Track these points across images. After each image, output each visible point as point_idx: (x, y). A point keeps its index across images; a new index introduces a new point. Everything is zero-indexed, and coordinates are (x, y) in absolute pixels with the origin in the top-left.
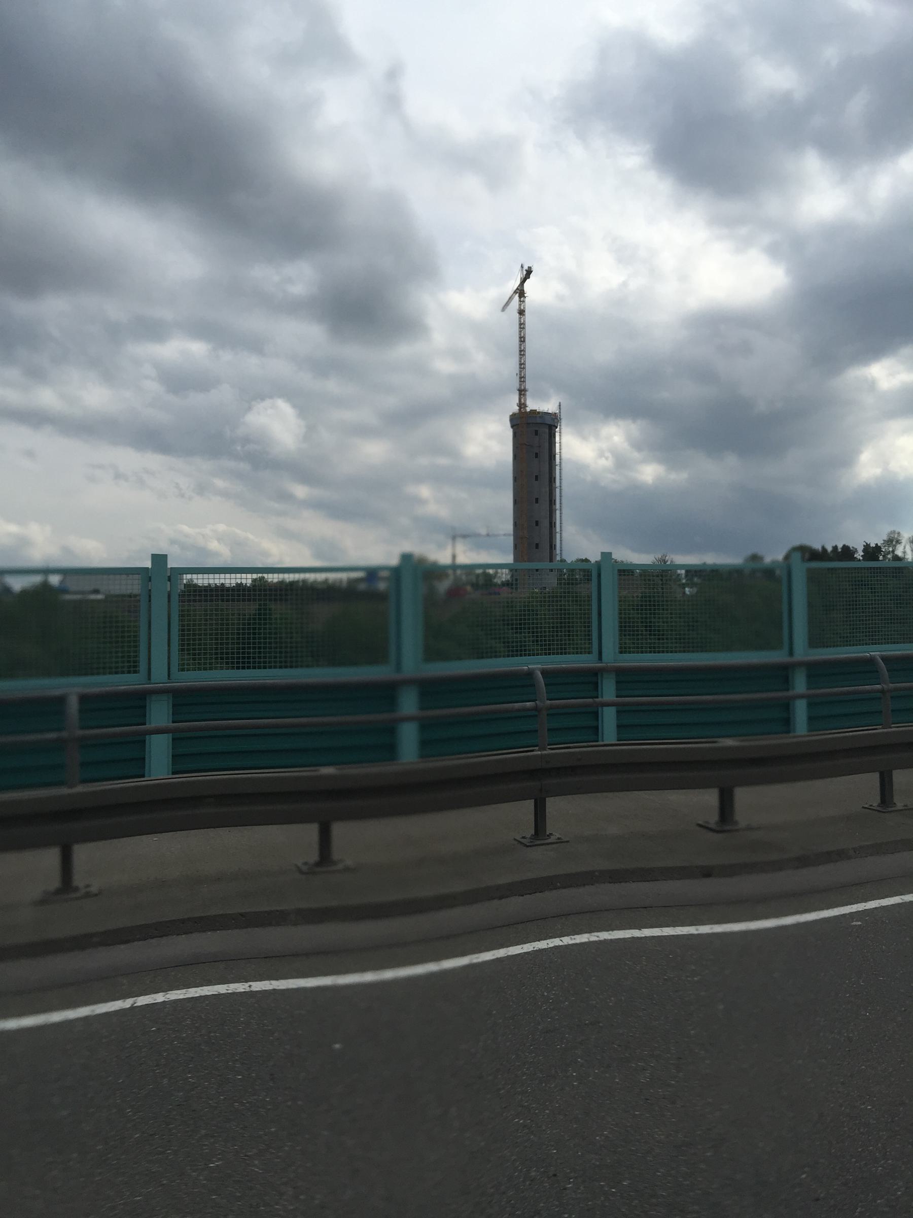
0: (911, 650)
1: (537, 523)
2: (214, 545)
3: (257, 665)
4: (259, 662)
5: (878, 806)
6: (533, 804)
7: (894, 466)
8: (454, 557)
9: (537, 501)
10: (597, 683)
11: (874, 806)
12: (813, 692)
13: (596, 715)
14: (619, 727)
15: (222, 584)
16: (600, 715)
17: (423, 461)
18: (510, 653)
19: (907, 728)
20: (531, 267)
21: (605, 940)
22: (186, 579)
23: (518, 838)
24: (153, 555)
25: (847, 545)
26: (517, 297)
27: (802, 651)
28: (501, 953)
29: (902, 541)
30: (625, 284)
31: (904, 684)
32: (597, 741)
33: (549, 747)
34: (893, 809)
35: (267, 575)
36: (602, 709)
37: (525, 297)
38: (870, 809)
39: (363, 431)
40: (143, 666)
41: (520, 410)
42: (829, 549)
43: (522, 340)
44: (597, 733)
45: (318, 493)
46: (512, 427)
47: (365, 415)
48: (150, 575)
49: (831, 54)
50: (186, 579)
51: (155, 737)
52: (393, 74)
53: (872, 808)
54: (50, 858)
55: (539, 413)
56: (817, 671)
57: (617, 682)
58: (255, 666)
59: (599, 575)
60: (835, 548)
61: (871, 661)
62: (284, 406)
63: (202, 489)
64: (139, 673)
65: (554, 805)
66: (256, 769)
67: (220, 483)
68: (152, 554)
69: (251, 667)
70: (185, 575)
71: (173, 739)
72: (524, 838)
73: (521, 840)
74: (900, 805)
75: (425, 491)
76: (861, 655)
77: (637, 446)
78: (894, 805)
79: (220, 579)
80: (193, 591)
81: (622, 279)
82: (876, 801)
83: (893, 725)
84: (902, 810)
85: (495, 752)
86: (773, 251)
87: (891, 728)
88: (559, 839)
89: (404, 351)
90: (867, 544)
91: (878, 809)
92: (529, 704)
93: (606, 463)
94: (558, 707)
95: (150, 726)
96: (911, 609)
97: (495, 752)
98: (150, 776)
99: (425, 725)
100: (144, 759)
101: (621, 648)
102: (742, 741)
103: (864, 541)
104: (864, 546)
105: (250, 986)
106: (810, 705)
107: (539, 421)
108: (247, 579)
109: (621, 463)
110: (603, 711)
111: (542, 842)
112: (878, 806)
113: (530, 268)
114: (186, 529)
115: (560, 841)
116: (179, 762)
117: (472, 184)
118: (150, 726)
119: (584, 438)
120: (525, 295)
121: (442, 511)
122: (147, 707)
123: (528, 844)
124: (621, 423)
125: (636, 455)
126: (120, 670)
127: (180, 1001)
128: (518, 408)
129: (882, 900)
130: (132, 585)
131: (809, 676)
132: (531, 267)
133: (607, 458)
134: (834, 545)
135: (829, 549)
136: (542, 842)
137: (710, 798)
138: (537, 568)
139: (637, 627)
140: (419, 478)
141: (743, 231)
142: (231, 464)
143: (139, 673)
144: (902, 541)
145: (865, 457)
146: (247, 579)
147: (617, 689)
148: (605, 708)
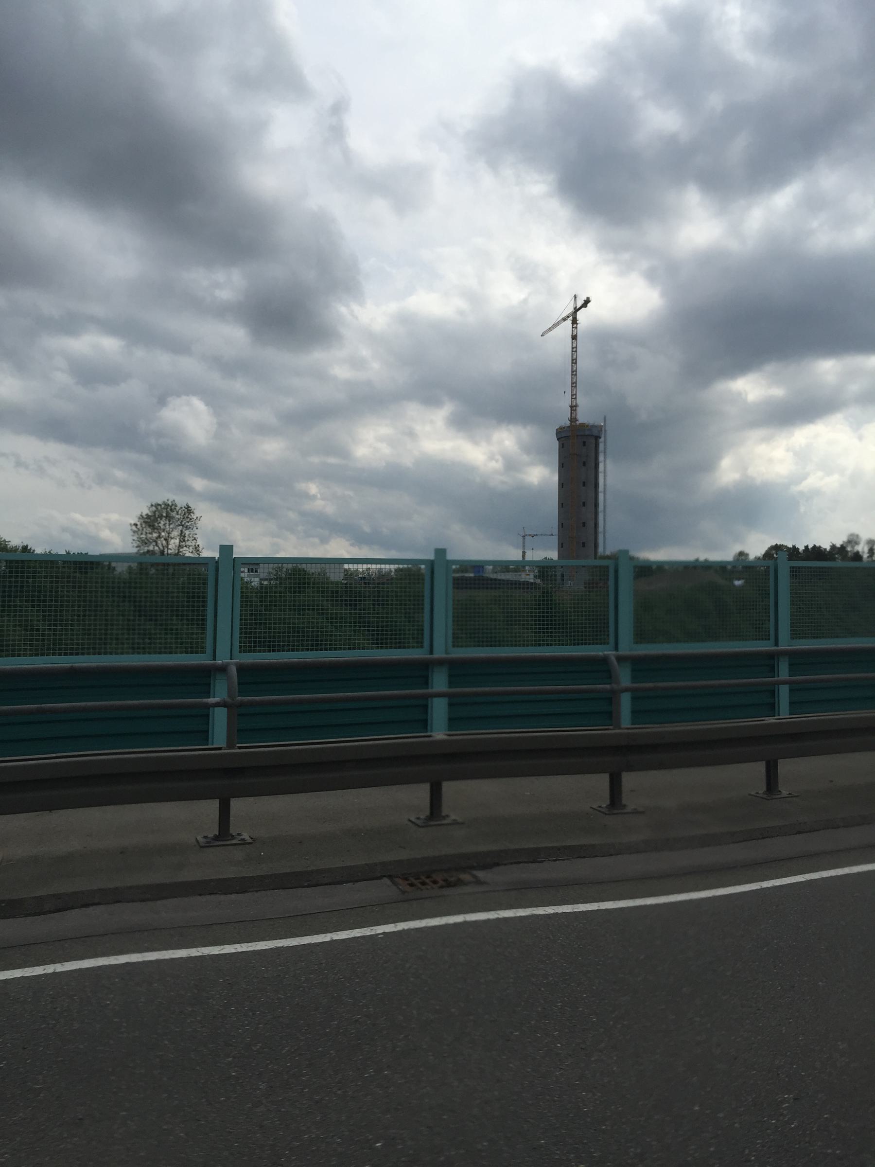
1: (584, 524)
2: (106, 534)
5: (763, 793)
6: (218, 802)
7: (752, 471)
9: (584, 504)
12: (635, 685)
13: (425, 708)
14: (791, 703)
17: (315, 460)
20: (589, 298)
21: (520, 916)
23: (413, 819)
24: (220, 546)
25: (817, 545)
26: (569, 322)
27: (786, 644)
28: (50, 969)
30: (525, 301)
33: (238, 745)
34: (779, 796)
37: (577, 324)
38: (756, 796)
39: (262, 430)
40: (426, 643)
41: (571, 424)
42: (801, 548)
43: (574, 361)
45: (215, 486)
46: (558, 439)
47: (265, 415)
49: (715, 101)
52: (338, 108)
53: (758, 795)
54: (213, 806)
55: (587, 426)
56: (798, 660)
57: (790, 665)
58: (67, 653)
59: (616, 571)
60: (807, 547)
62: (198, 403)
63: (102, 480)
64: (205, 653)
65: (629, 780)
67: (119, 474)
68: (220, 546)
69: (69, 654)
73: (755, 795)
75: (313, 488)
76: (542, 654)
77: (526, 449)
78: (779, 793)
81: (522, 296)
82: (762, 788)
85: (589, 728)
86: (651, 276)
89: (317, 356)
91: (765, 796)
92: (608, 686)
93: (497, 465)
94: (252, 704)
97: (589, 728)
99: (455, 703)
100: (207, 732)
102: (430, 736)
106: (634, 699)
107: (587, 433)
109: (511, 465)
110: (432, 702)
111: (619, 811)
112: (607, 807)
113: (588, 298)
114: (78, 516)
116: (236, 733)
117: (381, 206)
119: (476, 443)
120: (578, 322)
121: (330, 509)
122: (212, 686)
124: (511, 427)
125: (525, 458)
126: (22, 652)
128: (569, 422)
132: (589, 298)
133: (497, 461)
136: (619, 811)
138: (562, 565)
139: (527, 621)
140: (310, 476)
141: (626, 256)
142: (133, 456)
143: (205, 653)
145: (726, 463)
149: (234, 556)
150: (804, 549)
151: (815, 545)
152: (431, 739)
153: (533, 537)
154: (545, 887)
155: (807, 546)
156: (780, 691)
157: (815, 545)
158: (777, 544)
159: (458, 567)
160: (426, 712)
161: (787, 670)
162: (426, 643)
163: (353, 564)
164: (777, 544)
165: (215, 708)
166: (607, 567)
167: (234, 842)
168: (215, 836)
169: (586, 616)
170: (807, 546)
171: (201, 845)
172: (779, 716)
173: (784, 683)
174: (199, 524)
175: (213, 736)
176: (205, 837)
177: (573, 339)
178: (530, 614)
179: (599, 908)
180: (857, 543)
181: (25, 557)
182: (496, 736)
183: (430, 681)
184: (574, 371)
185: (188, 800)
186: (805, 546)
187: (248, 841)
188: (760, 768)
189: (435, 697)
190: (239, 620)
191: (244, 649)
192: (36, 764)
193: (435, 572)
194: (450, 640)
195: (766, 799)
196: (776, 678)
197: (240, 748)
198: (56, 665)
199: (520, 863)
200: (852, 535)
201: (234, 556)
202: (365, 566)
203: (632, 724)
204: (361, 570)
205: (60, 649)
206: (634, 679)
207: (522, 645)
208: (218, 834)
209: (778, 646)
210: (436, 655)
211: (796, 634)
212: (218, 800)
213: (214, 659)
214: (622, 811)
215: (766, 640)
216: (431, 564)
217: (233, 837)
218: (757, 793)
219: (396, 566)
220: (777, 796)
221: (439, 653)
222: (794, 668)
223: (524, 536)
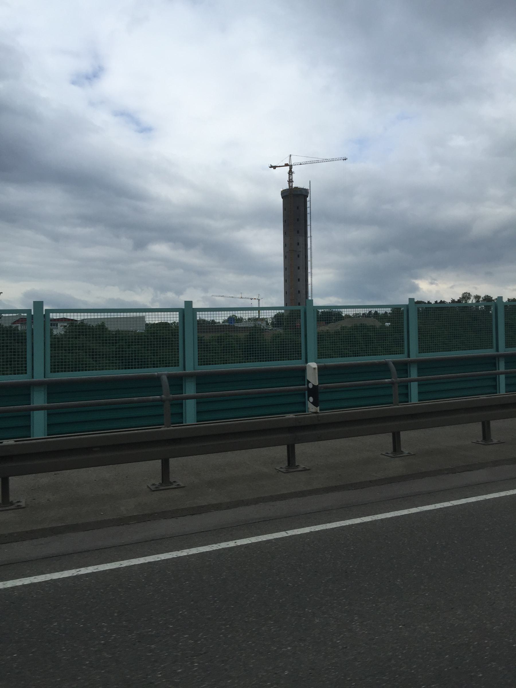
4: (276, 358)
5: (481, 441)
10: (407, 370)
11: (479, 442)
13: (495, 379)
14: (419, 393)
16: (184, 405)
18: (203, 363)
19: (446, 402)
22: (344, 314)
24: (502, 297)
29: (471, 298)
31: (483, 372)
35: (4, 314)
36: (410, 383)
44: (407, 397)
50: (344, 314)
59: (305, 313)
61: (386, 364)
66: (108, 430)
71: (197, 403)
72: (281, 468)
74: (495, 441)
78: (402, 453)
79: (74, 316)
80: (202, 323)
83: (399, 404)
84: (497, 443)
87: (398, 405)
88: (304, 468)
90: (453, 299)
95: (185, 395)
96: (1, 357)
98: (33, 437)
99: (51, 413)
101: (318, 355)
102: (16, 441)
103: (452, 298)
105: (338, 310)
108: (208, 317)
115: (305, 470)
118: (185, 395)
122: (184, 386)
123: (285, 472)
130: (117, 321)
131: (419, 369)
134: (436, 301)
135: (433, 302)
136: (294, 470)
137: (282, 451)
144: (471, 298)
146: (81, 316)
147: (418, 373)
152: (285, 417)
154: (280, 518)
155: (437, 301)
156: (500, 379)
161: (504, 367)
162: (495, 345)
165: (186, 400)
166: (300, 310)
167: (171, 487)
168: (160, 484)
169: (429, 336)
170: (437, 301)
171: (153, 489)
172: (411, 402)
173: (502, 373)
175: (411, 396)
176: (153, 485)
178: (371, 337)
179: (262, 540)
182: (207, 425)
183: (184, 388)
185: (344, 438)
186: (435, 301)
187: (23, 506)
188: (158, 463)
189: (501, 374)
191: (54, 369)
192: (214, 425)
193: (185, 316)
194: (197, 360)
195: (484, 444)
196: (183, 395)
197: (173, 427)
198: (241, 368)
199: (392, 483)
200: (465, 293)
202: (374, 309)
203: (419, 401)
205: (69, 368)
206: (506, 367)
207: (252, 362)
208: (161, 482)
209: (410, 358)
210: (36, 379)
211: (422, 349)
212: (161, 460)
213: (185, 370)
214: (296, 470)
215: (175, 366)
216: (407, 306)
217: (171, 484)
218: (387, 453)
219: (278, 311)
220: (490, 443)
221: (189, 370)
222: (420, 371)
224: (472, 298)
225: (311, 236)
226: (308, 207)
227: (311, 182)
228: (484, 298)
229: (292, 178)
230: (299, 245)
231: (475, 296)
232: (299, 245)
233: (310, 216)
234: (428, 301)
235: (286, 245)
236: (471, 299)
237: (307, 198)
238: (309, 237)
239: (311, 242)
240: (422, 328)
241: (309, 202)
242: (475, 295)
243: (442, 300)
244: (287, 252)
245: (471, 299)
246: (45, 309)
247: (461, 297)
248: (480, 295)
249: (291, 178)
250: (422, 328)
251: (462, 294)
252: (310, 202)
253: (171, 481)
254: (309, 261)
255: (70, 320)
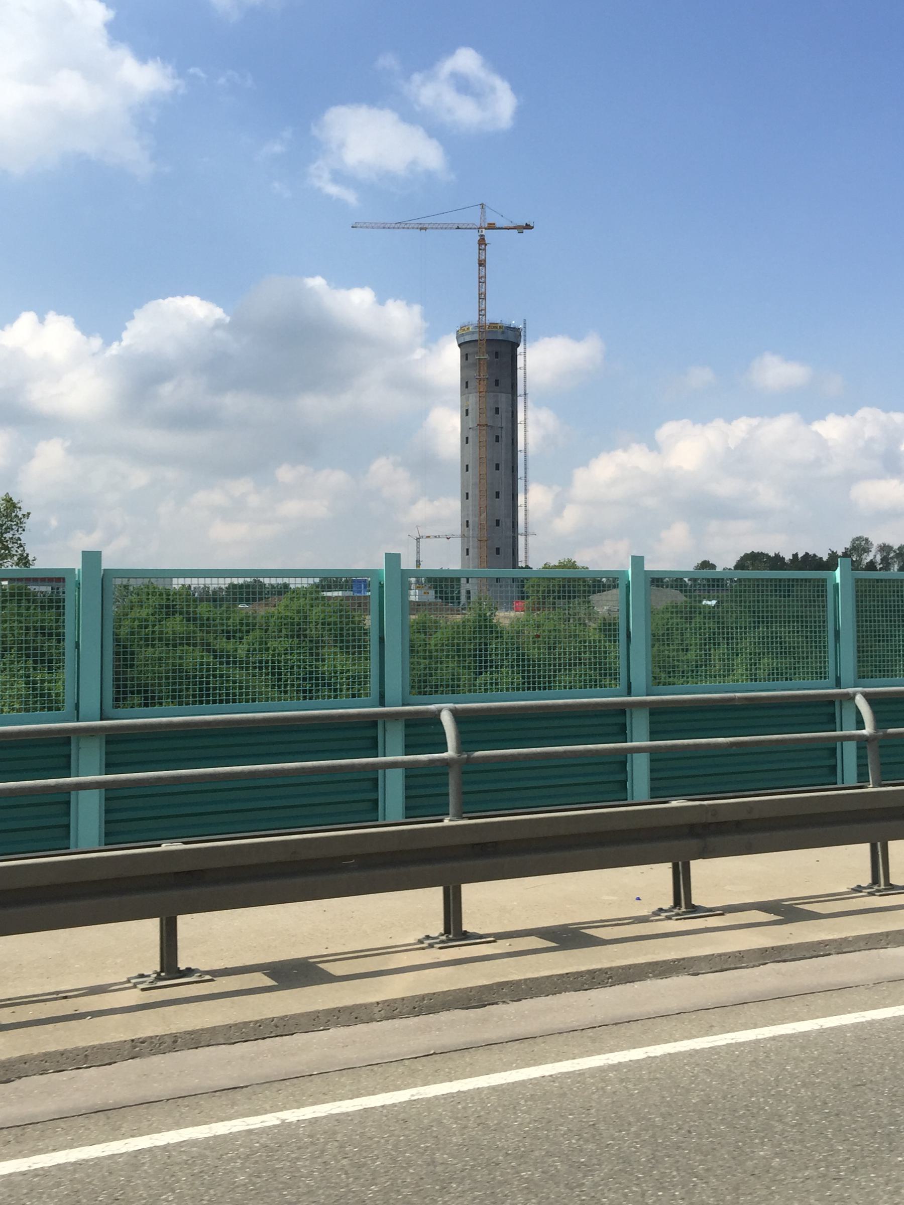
0: (903, 686)
3: (150, 695)
8: (418, 563)
15: (507, 611)
24: (83, 552)
25: (811, 553)
32: (836, 783)
36: (632, 755)
37: (486, 245)
42: (788, 557)
48: (77, 579)
51: (83, 794)
60: (795, 556)
68: (83, 552)
70: (417, 600)
85: (769, 791)
90: (833, 552)
104: (829, 554)
127: (361, 1094)
129: (698, 1048)
148: (635, 755)
149: (103, 568)
150: (791, 558)
151: (807, 554)
153: (448, 538)
155: (797, 554)
157: (807, 554)
158: (753, 552)
159: (317, 580)
160: (68, 814)
163: (185, 578)
164: (753, 552)
170: (797, 554)
174: (28, 523)
177: (480, 265)
180: (867, 550)
181: (569, 573)
184: (482, 310)
186: (793, 555)
190: (66, 649)
200: (858, 539)
201: (103, 568)
204: (292, 586)
219: (228, 581)
223: (419, 539)
224: (874, 550)
225: (525, 394)
226: (520, 368)
227: (527, 322)
228: (898, 552)
229: (485, 258)
230: (498, 414)
231: (881, 546)
232: (498, 414)
233: (525, 484)
234: (775, 554)
235: (469, 411)
236: (871, 551)
237: (518, 349)
238: (520, 478)
239: (525, 469)
240: (46, 631)
241: (523, 356)
242: (880, 542)
243: (808, 552)
244: (470, 428)
245: (870, 553)
246: (104, 570)
247: (848, 546)
248: (891, 545)
249: (483, 257)
250: (46, 631)
251: (851, 540)
252: (525, 481)
253: (179, 968)
254: (520, 451)
255: (47, 579)
